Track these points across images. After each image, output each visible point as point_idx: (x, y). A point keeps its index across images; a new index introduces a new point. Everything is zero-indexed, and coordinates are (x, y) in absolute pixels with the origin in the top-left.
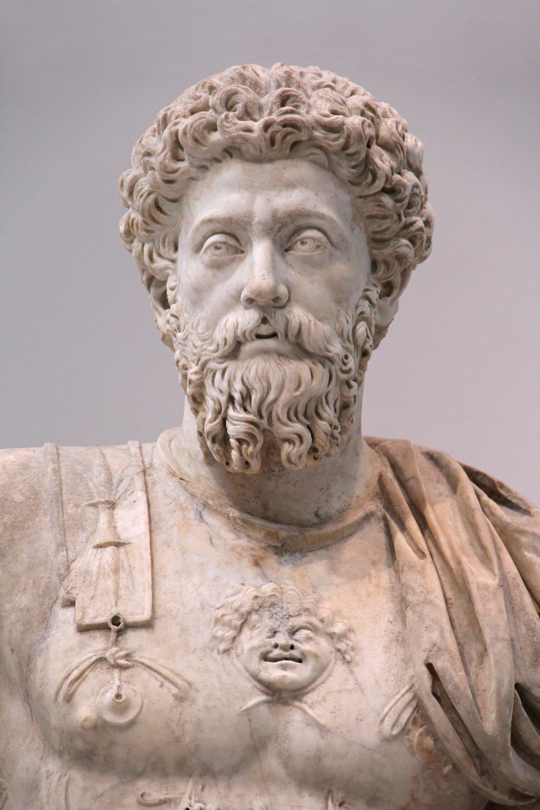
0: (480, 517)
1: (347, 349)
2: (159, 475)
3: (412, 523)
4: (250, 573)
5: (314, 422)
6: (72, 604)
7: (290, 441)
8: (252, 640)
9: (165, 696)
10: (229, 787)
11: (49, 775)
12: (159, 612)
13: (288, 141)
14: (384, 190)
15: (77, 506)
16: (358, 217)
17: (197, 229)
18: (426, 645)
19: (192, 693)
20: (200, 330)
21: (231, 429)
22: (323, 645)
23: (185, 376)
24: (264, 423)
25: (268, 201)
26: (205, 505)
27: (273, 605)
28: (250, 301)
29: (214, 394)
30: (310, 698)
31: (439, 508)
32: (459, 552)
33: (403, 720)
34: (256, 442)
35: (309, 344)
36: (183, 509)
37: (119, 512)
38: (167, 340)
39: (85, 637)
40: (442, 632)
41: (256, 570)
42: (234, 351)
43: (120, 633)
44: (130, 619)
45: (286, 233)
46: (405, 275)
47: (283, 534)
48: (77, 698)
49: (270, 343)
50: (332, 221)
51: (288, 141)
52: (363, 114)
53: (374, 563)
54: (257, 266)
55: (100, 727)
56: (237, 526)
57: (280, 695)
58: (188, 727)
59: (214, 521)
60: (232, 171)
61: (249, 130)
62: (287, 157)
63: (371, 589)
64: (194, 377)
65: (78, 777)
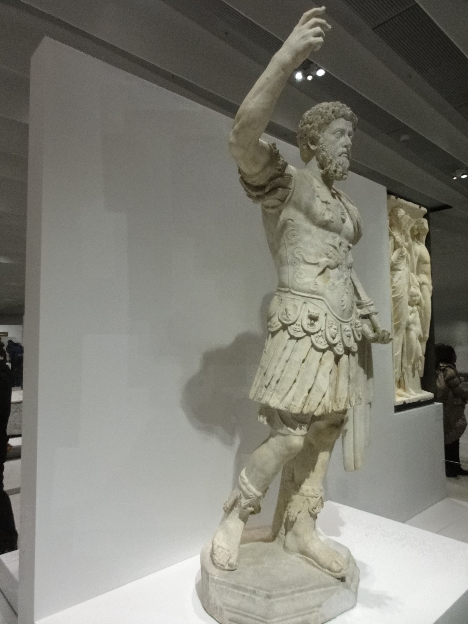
60: (342, 120)
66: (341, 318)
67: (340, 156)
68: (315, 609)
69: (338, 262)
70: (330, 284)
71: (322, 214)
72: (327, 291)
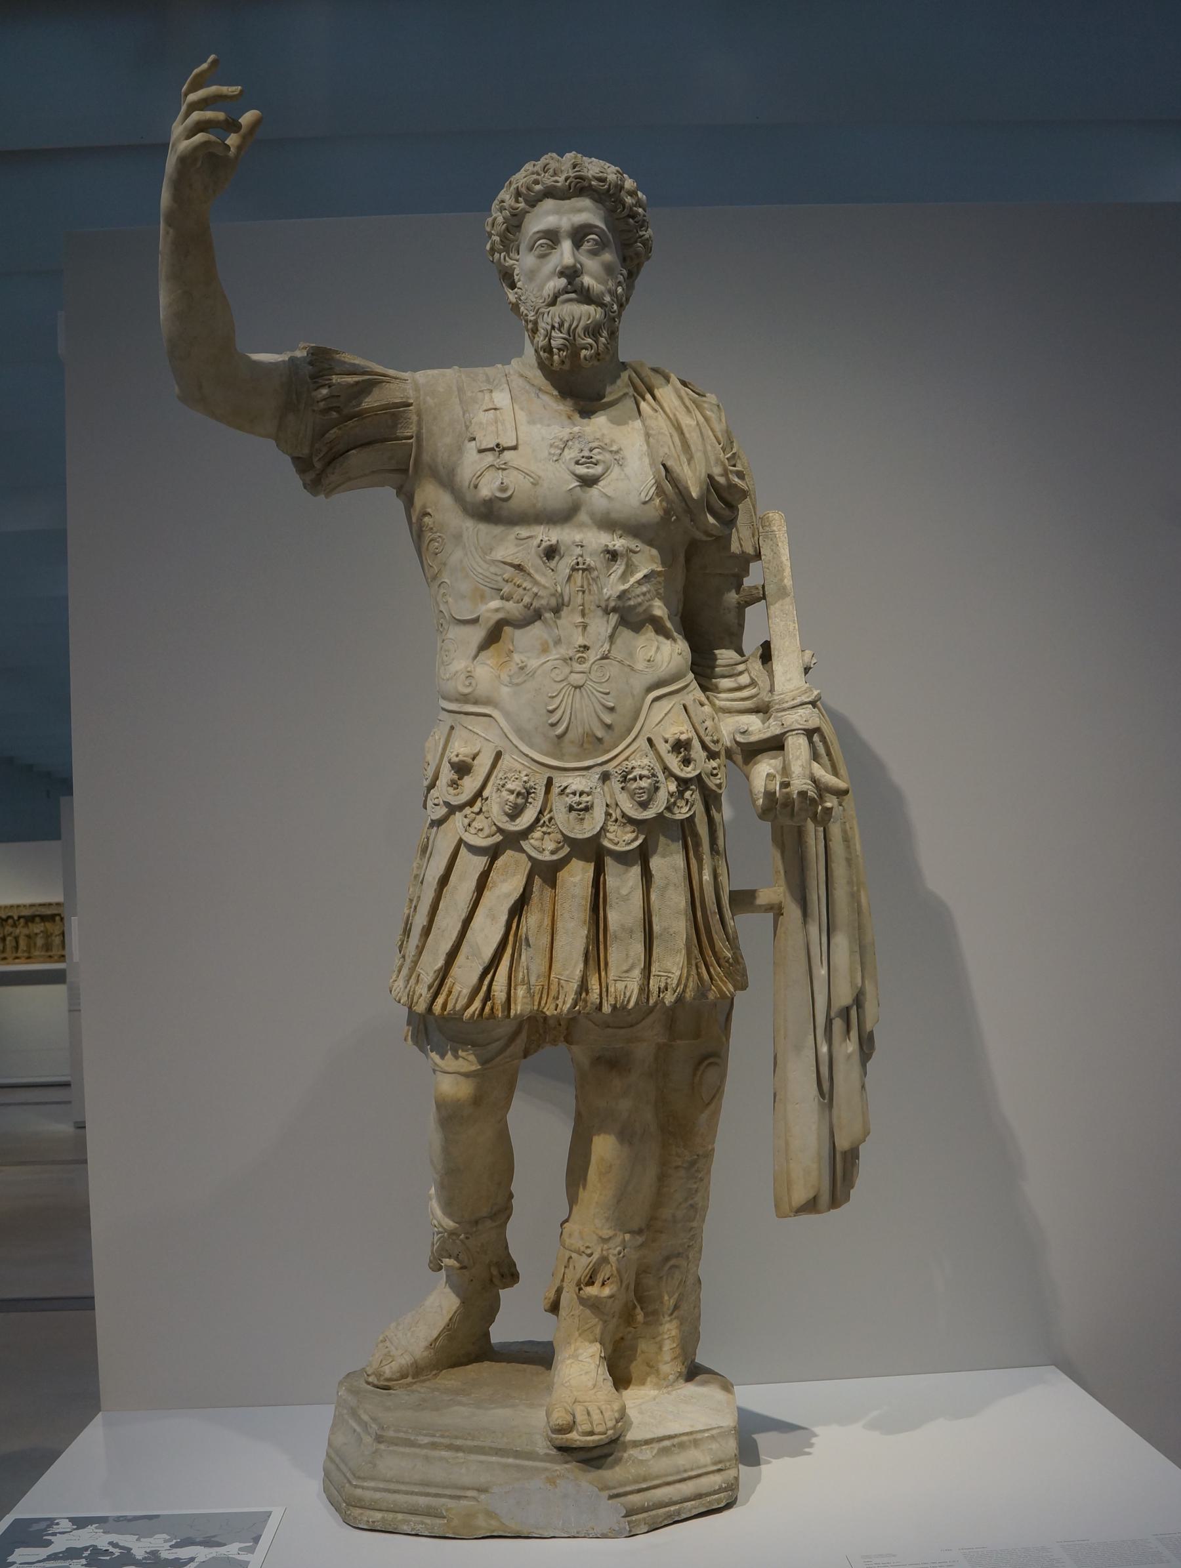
3: (648, 396)
4: (567, 422)
6: (474, 439)
7: (586, 349)
8: (570, 454)
9: (526, 483)
11: (467, 528)
13: (580, 188)
14: (629, 216)
18: (661, 454)
22: (608, 456)
33: (651, 493)
37: (494, 394)
38: (515, 307)
44: (505, 445)
45: (579, 235)
49: (573, 296)
54: (566, 253)
59: (546, 398)
60: (549, 203)
65: (483, 528)
67: (553, 303)
68: (470, 1493)
69: (536, 604)
70: (514, 668)
72: (505, 691)
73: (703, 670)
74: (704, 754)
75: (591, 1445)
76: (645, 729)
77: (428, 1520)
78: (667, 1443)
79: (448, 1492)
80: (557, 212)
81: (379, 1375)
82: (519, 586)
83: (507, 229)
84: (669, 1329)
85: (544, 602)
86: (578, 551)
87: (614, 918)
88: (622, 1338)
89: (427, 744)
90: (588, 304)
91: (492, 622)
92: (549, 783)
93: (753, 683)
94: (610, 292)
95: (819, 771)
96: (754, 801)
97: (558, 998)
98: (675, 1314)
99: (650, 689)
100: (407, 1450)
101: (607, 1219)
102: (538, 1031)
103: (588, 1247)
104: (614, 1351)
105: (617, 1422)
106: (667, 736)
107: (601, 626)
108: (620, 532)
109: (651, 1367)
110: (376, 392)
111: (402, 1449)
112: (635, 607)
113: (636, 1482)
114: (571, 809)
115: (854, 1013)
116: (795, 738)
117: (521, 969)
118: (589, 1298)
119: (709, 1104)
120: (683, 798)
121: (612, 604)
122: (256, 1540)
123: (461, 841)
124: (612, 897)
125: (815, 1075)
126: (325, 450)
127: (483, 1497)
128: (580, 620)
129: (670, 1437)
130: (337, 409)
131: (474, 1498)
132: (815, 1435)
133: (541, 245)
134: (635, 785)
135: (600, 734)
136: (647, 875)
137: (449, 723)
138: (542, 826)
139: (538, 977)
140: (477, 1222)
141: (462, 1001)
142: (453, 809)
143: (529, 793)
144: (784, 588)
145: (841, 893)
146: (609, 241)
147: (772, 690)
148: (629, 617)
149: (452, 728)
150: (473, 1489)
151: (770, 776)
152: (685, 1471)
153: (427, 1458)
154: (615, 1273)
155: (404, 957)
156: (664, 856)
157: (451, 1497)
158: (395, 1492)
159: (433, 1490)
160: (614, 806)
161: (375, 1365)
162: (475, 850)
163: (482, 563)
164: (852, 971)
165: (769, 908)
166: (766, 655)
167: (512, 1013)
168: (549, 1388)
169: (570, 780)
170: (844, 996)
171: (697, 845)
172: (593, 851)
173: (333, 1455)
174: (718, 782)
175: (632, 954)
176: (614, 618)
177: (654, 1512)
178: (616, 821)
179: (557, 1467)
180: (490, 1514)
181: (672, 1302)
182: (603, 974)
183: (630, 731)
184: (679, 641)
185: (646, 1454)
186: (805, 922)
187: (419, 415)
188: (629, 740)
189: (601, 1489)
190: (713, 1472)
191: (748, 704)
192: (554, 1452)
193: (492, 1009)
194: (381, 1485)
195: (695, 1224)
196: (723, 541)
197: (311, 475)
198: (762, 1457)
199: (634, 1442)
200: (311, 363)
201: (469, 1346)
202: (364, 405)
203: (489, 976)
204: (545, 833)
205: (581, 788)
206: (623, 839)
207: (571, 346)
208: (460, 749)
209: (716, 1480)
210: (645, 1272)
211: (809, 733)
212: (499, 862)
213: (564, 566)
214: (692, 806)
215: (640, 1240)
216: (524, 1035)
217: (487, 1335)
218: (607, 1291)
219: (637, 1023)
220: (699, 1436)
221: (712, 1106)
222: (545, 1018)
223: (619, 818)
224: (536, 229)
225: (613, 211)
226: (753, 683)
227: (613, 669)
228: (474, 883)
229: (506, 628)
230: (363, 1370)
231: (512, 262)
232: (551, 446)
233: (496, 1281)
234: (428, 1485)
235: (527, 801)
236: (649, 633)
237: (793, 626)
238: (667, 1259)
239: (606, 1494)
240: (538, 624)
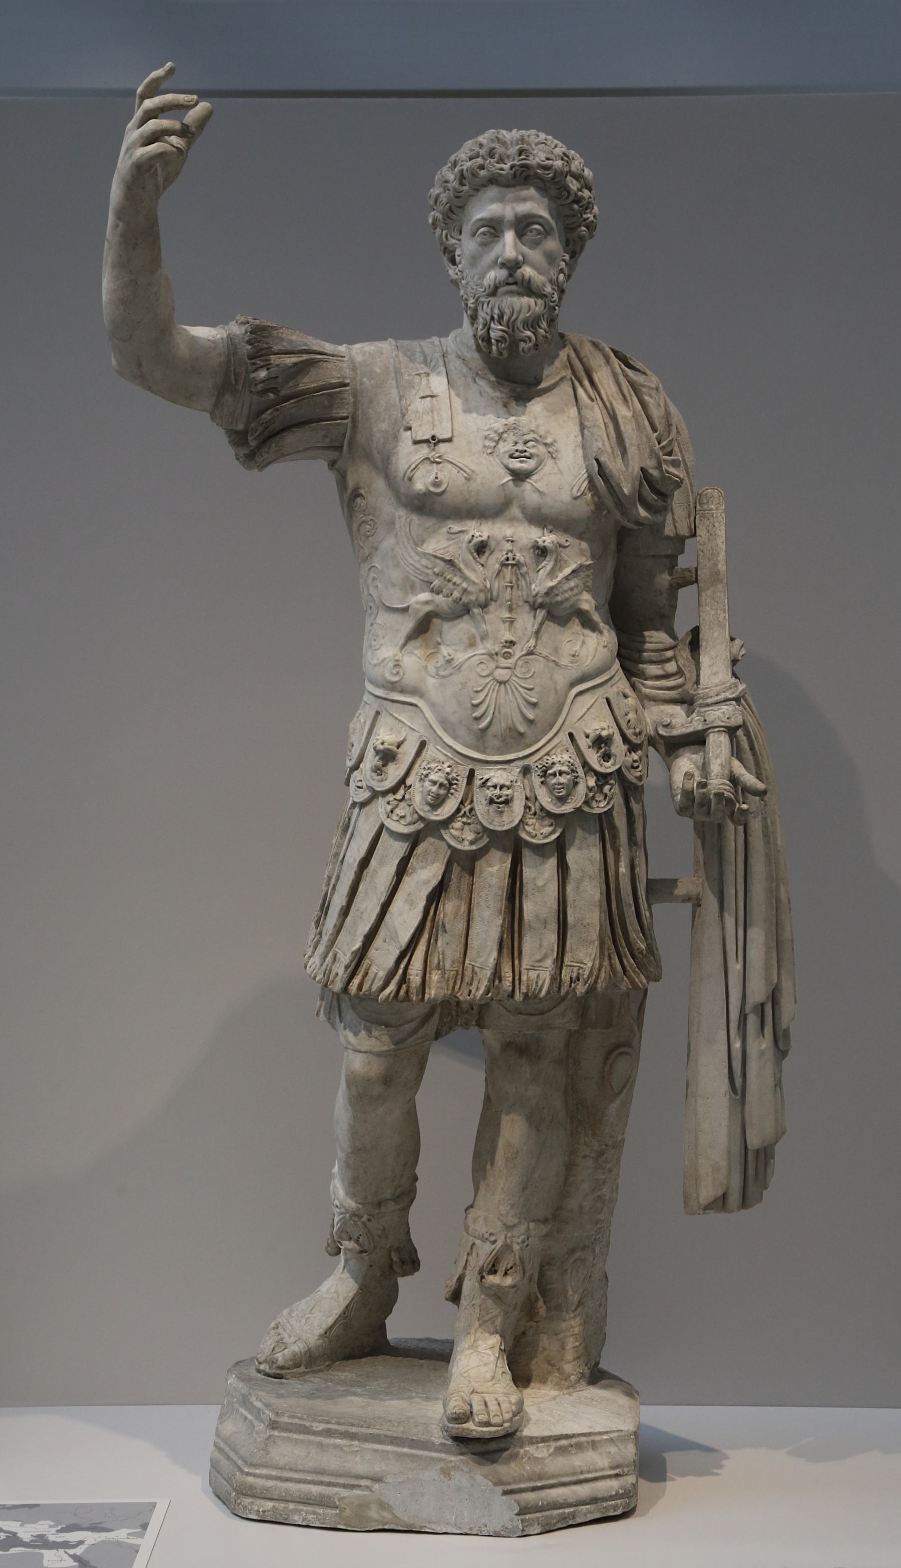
0: (622, 379)
1: (553, 289)
2: (452, 357)
4: (502, 411)
5: (537, 330)
6: (410, 429)
7: (525, 341)
8: (505, 447)
9: (459, 479)
10: (494, 524)
12: (455, 433)
13: (523, 176)
15: (409, 375)
16: (557, 214)
17: (474, 224)
18: (595, 449)
19: (474, 476)
20: (475, 280)
21: (492, 334)
22: (542, 449)
23: (466, 305)
24: (510, 331)
25: (513, 209)
26: (477, 374)
27: (515, 428)
28: (503, 265)
29: (482, 315)
30: (534, 478)
31: (599, 374)
32: (611, 398)
33: (583, 489)
34: (506, 341)
35: (534, 286)
36: (465, 376)
38: (456, 283)
39: (418, 446)
40: (603, 442)
41: (505, 409)
42: (494, 291)
43: (435, 445)
44: (441, 437)
46: (582, 247)
47: (519, 390)
48: (415, 478)
49: (514, 287)
50: (546, 219)
51: (523, 176)
52: (562, 159)
53: (566, 405)
54: (509, 242)
55: (428, 494)
56: (493, 385)
57: (519, 477)
58: (472, 494)
59: (482, 383)
61: (502, 169)
62: (522, 184)
63: (565, 418)
64: (472, 306)
65: (415, 518)
66: (476, 749)
68: (363, 1483)
69: (465, 599)
70: (441, 661)
71: (406, 479)
72: (431, 682)
73: (629, 658)
74: (625, 748)
75: (487, 1436)
76: (566, 723)
77: (320, 1511)
78: (564, 1442)
79: (341, 1481)
80: (501, 200)
81: (272, 1362)
82: (449, 581)
83: (451, 210)
84: (572, 1326)
85: (473, 598)
86: (508, 546)
87: (529, 908)
88: (524, 1333)
89: (351, 725)
90: (529, 296)
91: (421, 614)
92: (471, 775)
93: (680, 672)
94: (551, 281)
95: (738, 769)
96: (673, 796)
97: (471, 984)
98: (579, 1311)
99: (573, 685)
100: (302, 1437)
101: (512, 1206)
102: (451, 1016)
103: (491, 1234)
104: (515, 1346)
105: (514, 1415)
106: (588, 731)
107: (527, 622)
108: (550, 527)
109: (553, 1365)
110: (313, 372)
111: (295, 1436)
112: (562, 602)
113: (530, 1479)
114: (491, 801)
115: (768, 1009)
116: (716, 735)
117: (436, 954)
118: (492, 1286)
119: (620, 1093)
120: (602, 792)
121: (540, 600)
122: (145, 1526)
123: (382, 826)
124: (528, 888)
125: (726, 1071)
126: (260, 429)
127: (377, 1486)
128: (507, 615)
129: (567, 1437)
130: (274, 390)
131: (368, 1488)
132: (727, 1458)
133: (484, 234)
134: (554, 781)
135: (522, 729)
136: (563, 868)
137: (376, 707)
138: (462, 816)
139: (453, 962)
140: (379, 1204)
141: (378, 984)
142: (376, 794)
143: (451, 784)
144: (718, 573)
145: (758, 888)
146: (552, 228)
147: (697, 682)
148: (555, 611)
149: (378, 713)
150: (367, 1478)
151: (689, 776)
152: (582, 1473)
153: (321, 1446)
154: (518, 1262)
155: (320, 934)
156: (580, 849)
157: (344, 1486)
158: (287, 1480)
159: (326, 1479)
160: (533, 799)
161: (267, 1352)
162: (394, 835)
163: (413, 554)
164: (767, 968)
165: (687, 899)
166: (695, 643)
167: (427, 997)
168: (446, 1382)
169: (491, 774)
170: (758, 992)
171: (615, 837)
172: (513, 845)
173: (222, 1445)
174: (639, 774)
175: (545, 944)
176: (541, 614)
177: (548, 1513)
178: (535, 814)
179: (453, 1458)
180: (383, 1506)
181: (576, 1298)
182: (516, 962)
183: (551, 726)
184: (606, 633)
185: (541, 1451)
186: (721, 916)
187: (355, 396)
188: (555, 730)
189: (495, 1484)
190: (610, 1477)
191: (672, 694)
192: (449, 1442)
193: (407, 992)
194: (274, 1473)
195: (602, 1216)
196: (657, 529)
197: (244, 451)
198: (668, 1475)
199: (531, 1438)
200: (249, 342)
201: (360, 1341)
202: (302, 387)
203: (406, 960)
204: (465, 823)
205: (502, 781)
206: (541, 833)
207: (512, 341)
208: (385, 736)
209: (613, 1485)
210: (549, 1263)
211: (731, 731)
212: (420, 849)
213: (493, 561)
214: (611, 799)
215: (545, 1229)
216: (436, 1017)
217: (383, 1327)
218: (509, 1281)
219: (548, 1011)
220: (598, 1438)
221: (623, 1095)
222: (458, 1003)
223: (538, 811)
224: (479, 216)
225: (558, 198)
226: (680, 672)
227: (538, 664)
228: (393, 869)
229: (435, 620)
230: (252, 1359)
231: (454, 241)
232: (486, 438)
233: (397, 1268)
234: (322, 1472)
235: (448, 792)
236: (575, 625)
237: (724, 616)
238: (573, 1251)
239: (500, 1489)
240: (466, 617)
